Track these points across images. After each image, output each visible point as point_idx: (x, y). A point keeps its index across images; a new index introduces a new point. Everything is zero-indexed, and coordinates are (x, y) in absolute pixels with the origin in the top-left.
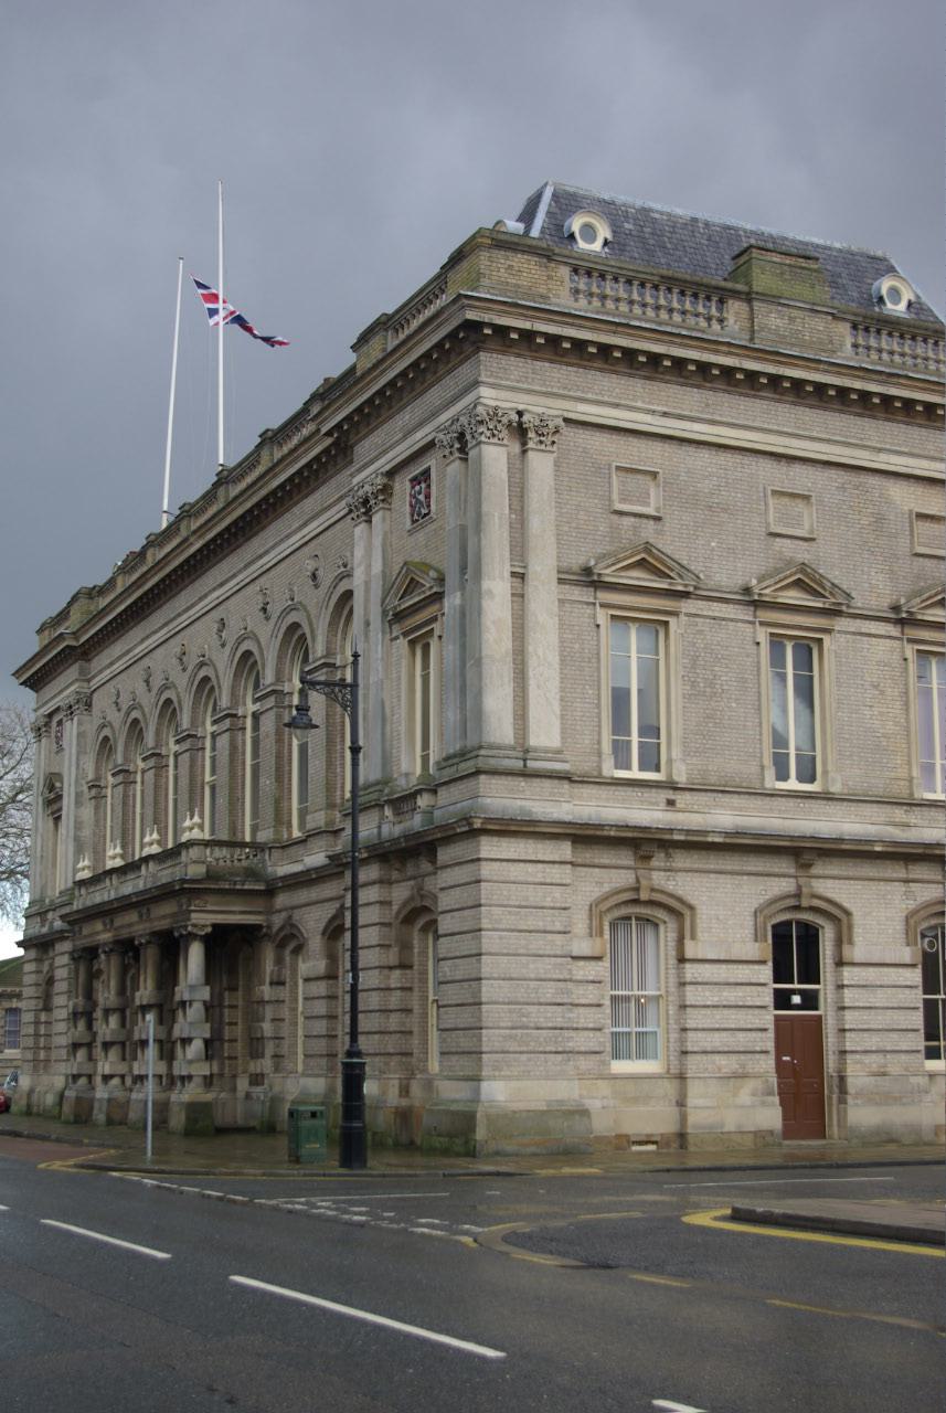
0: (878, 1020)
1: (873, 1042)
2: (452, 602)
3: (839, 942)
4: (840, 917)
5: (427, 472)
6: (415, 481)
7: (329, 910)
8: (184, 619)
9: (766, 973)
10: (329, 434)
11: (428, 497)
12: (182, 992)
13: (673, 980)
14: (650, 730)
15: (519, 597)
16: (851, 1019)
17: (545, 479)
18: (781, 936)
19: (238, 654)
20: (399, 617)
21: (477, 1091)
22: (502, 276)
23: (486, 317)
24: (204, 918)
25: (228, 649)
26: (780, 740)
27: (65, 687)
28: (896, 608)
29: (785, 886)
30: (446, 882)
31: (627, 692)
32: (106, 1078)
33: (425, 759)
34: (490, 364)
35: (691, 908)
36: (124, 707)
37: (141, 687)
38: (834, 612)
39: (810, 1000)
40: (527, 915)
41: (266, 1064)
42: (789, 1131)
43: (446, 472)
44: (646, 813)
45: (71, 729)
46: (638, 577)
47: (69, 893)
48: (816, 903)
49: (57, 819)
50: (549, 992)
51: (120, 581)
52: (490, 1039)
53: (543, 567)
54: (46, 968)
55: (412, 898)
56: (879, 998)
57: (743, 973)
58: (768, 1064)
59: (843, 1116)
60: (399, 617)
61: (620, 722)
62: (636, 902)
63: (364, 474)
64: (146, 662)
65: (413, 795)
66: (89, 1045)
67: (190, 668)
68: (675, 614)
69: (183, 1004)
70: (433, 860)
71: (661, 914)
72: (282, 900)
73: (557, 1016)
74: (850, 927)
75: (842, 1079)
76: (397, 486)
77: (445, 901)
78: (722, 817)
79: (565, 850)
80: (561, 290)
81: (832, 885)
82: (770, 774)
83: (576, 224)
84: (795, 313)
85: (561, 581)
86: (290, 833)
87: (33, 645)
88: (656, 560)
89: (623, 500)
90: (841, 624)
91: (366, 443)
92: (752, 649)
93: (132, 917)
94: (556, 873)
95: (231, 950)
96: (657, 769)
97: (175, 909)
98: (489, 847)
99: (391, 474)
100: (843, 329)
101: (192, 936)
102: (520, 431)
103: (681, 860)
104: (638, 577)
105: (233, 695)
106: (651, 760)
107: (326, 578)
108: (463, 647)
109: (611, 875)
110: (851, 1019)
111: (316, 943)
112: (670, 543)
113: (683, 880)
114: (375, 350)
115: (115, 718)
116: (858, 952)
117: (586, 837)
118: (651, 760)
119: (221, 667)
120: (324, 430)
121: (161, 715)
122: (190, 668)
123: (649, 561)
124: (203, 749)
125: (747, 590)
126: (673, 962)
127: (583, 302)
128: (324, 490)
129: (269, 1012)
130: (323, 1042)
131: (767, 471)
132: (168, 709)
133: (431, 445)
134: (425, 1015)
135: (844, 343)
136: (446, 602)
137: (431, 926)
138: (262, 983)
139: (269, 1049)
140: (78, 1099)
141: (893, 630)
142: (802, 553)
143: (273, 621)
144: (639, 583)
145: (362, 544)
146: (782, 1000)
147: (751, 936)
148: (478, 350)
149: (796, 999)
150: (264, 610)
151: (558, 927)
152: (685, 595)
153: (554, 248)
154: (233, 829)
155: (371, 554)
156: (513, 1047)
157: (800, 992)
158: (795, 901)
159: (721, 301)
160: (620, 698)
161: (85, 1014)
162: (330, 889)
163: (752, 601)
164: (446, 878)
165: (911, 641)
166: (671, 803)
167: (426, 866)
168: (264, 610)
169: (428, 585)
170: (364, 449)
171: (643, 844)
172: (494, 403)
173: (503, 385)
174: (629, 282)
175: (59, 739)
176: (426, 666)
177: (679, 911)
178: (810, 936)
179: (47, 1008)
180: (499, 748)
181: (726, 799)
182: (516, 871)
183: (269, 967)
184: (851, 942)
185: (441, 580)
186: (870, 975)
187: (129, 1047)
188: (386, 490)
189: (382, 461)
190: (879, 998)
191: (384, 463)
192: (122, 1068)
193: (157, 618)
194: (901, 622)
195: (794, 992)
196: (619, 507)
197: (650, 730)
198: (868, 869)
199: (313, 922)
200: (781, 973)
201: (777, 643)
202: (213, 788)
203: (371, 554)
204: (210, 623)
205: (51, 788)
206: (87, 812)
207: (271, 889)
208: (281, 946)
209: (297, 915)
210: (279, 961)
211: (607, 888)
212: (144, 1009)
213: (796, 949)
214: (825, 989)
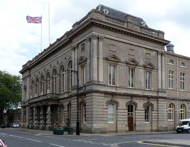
0: (140, 117)
1: (139, 120)
2: (88, 61)
3: (135, 107)
4: (136, 105)
5: (84, 44)
6: (82, 45)
7: (68, 102)
8: (59, 56)
9: (127, 111)
10: (69, 38)
11: (84, 47)
12: (47, 113)
13: (116, 112)
14: (114, 80)
15: (98, 61)
16: (137, 117)
17: (99, 47)
18: (129, 106)
19: (69, 60)
20: (80, 64)
21: (92, 125)
22: (96, 16)
23: (95, 21)
24: (50, 103)
25: (52, 68)
26: (129, 82)
27: (27, 74)
28: (144, 65)
29: (129, 100)
30: (87, 99)
31: (111, 74)
32: (36, 124)
33: (83, 83)
34: (94, 28)
35: (118, 103)
36: (36, 76)
37: (38, 74)
38: (136, 65)
39: (132, 114)
40: (97, 103)
41: (58, 122)
42: (129, 130)
43: (87, 44)
44: (113, 90)
45: (28, 79)
46: (113, 59)
47: (29, 100)
48: (133, 102)
49: (26, 91)
50: (101, 113)
51: (35, 60)
52: (94, 119)
53: (101, 57)
54: (25, 110)
55: (82, 101)
56: (140, 114)
57: (124, 111)
58: (127, 122)
59: (135, 129)
60: (80, 64)
61: (110, 79)
62: (111, 102)
63: (74, 43)
64: (45, 67)
65: (82, 87)
66: (33, 119)
67: (46, 71)
68: (117, 64)
69: (48, 114)
70: (85, 96)
71: (115, 103)
72: (61, 101)
73: (102, 116)
74: (137, 105)
75: (135, 124)
76: (79, 46)
77: (87, 101)
78: (123, 91)
79: (103, 95)
80: (103, 19)
81: (136, 100)
82: (128, 85)
83: (104, 10)
84: (133, 25)
85: (103, 59)
86: (61, 92)
87: (21, 68)
88: (41, 89)
89: (111, 49)
90: (137, 67)
91: (74, 40)
92: (126, 69)
93: (40, 103)
94: (103, 98)
95: (54, 108)
96: (114, 85)
97: (46, 102)
98: (94, 94)
99: (78, 44)
100: (139, 28)
101: (49, 106)
102: (98, 38)
103: (117, 96)
104: (113, 59)
105: (53, 75)
106: (114, 84)
107: (67, 59)
108: (90, 68)
109: (109, 98)
110: (137, 117)
111: (66, 107)
112: (117, 55)
113: (118, 99)
114: (76, 27)
115: (34, 78)
116: (138, 109)
117: (106, 93)
118: (114, 84)
119: (51, 71)
120: (68, 38)
121: (69, 64)
122: (46, 71)
123: (114, 57)
124: (70, 72)
125: (126, 62)
126: (116, 109)
127: (106, 21)
128: (67, 47)
129: (59, 115)
130: (157, 112)
131: (128, 46)
132: (42, 77)
133: (85, 40)
134: (83, 116)
135: (138, 29)
136: (87, 62)
137: (85, 105)
138: (58, 112)
139: (59, 120)
140: (31, 126)
141: (143, 68)
142: (133, 57)
143: (59, 65)
144: (113, 60)
145: (74, 54)
146: (129, 114)
147: (125, 106)
148: (93, 26)
149: (130, 114)
150: (57, 63)
151: (102, 105)
152: (119, 62)
153: (102, 13)
154: (53, 92)
155: (75, 56)
156: (96, 120)
157: (131, 113)
158: (131, 102)
159: (124, 22)
160: (110, 75)
161: (38, 115)
162: (69, 100)
163: (127, 63)
164: (87, 98)
165: (145, 69)
166: (116, 89)
167: (84, 97)
168: (57, 63)
169: (84, 59)
170: (74, 41)
171: (113, 94)
172: (95, 34)
173: (95, 32)
174: (112, 19)
175: (26, 80)
176: (83, 70)
177: (117, 103)
178: (132, 106)
179: (25, 115)
180: (95, 81)
181: (123, 89)
182: (98, 97)
183: (59, 110)
184: (137, 107)
185: (86, 59)
186: (139, 111)
187: (39, 120)
188: (78, 47)
189: (77, 42)
190: (140, 114)
191: (77, 43)
192: (38, 122)
193: (41, 64)
194: (144, 67)
195: (130, 113)
196: (110, 49)
197: (114, 80)
198: (139, 98)
199: (66, 104)
200: (129, 111)
201: (129, 69)
202: (49, 87)
203: (75, 56)
204: (49, 65)
205: (25, 87)
206: (31, 90)
207: (59, 100)
208: (60, 107)
209: (63, 103)
210: (60, 109)
211: (108, 100)
212: (41, 115)
213: (130, 108)
214: (134, 113)
